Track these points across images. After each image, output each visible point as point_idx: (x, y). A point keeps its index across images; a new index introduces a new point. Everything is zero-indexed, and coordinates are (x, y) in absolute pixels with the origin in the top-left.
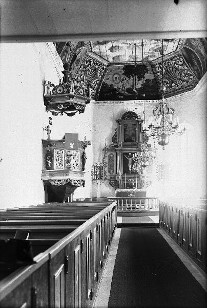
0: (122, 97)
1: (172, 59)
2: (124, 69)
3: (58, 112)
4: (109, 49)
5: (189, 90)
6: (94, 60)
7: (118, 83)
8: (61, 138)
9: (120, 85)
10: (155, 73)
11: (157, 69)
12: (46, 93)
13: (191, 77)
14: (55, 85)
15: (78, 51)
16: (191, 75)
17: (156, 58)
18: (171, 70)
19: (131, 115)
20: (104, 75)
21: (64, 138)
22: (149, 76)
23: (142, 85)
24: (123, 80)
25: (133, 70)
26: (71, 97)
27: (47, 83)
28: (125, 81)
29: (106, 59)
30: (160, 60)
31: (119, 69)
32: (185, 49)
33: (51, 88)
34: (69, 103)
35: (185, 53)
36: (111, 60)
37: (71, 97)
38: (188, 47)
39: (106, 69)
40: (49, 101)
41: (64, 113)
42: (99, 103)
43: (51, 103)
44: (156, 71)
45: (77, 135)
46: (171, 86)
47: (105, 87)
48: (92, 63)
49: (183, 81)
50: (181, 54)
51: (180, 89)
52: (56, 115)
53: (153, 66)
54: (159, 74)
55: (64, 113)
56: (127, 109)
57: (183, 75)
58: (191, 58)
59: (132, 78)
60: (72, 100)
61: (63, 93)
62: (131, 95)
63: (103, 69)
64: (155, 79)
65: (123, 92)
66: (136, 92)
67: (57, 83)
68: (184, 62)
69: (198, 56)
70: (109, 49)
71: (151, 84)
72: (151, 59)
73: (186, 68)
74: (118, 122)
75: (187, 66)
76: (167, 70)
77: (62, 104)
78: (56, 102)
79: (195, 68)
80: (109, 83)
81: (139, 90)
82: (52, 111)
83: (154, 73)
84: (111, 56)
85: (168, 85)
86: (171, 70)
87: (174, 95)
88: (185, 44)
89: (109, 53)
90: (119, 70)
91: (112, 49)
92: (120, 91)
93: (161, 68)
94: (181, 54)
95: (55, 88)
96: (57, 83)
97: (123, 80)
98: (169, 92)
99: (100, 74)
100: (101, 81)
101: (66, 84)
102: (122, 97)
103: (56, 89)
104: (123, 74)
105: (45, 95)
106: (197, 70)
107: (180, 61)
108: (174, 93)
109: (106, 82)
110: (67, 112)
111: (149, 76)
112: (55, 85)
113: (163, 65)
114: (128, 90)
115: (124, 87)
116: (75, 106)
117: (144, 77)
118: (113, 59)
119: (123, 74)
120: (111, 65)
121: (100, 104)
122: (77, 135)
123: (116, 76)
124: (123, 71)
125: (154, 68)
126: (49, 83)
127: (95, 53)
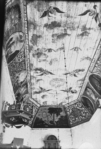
0: (47, 126)
1: (75, 104)
2: (48, 109)
3: (10, 125)
4: (42, 97)
5: (87, 121)
6: (32, 103)
7: (45, 118)
8: (10, 143)
9: (46, 119)
10: (66, 112)
11: (67, 110)
12: (4, 109)
13: (87, 114)
14: (10, 104)
15: (24, 96)
16: (87, 113)
17: (67, 103)
18: (75, 110)
19: (52, 138)
20: (37, 112)
21: (12, 143)
22: (62, 114)
23: (59, 119)
24: (48, 116)
25: (54, 110)
26: (21, 112)
27: (5, 103)
28: (49, 117)
29: (39, 103)
30: (93, 64)
31: (46, 109)
32: (83, 97)
33: (8, 106)
34: (19, 116)
35: (83, 101)
36: (42, 104)
37: (21, 112)
38: (84, 96)
39: (38, 110)
40: (5, 115)
41: (13, 126)
42: (33, 129)
43: (6, 116)
44: (67, 111)
45: (22, 140)
46: (75, 120)
47: (37, 120)
48: (31, 105)
49: (82, 116)
50: (81, 101)
51: (81, 121)
52: (8, 127)
53: (65, 108)
54: (68, 113)
55: (13, 126)
56: (49, 134)
57: (82, 113)
58: (86, 102)
59: (53, 114)
60: (21, 114)
61: (15, 109)
62: (52, 125)
63: (37, 109)
64: (66, 116)
65: (48, 123)
66: (55, 123)
67: (12, 103)
68: (82, 105)
69: (91, 101)
70: (42, 97)
71: (64, 119)
72: (63, 104)
73: (83, 109)
74: (44, 142)
75: (84, 108)
76: (73, 111)
77: (14, 117)
78: (9, 116)
79: (89, 108)
80: (40, 117)
81: (57, 122)
82: (6, 124)
83: (65, 112)
84: (42, 101)
85: (74, 119)
86: (75, 110)
87: (78, 125)
88: (83, 95)
89: (41, 99)
90: (46, 110)
91: (43, 97)
92: (46, 122)
93: (69, 109)
94: (81, 101)
95: (11, 106)
96: (12, 103)
97: (48, 116)
98: (74, 124)
99: (35, 112)
100: (35, 116)
101: (18, 104)
102: (47, 126)
103: (11, 107)
104: (48, 112)
105: (3, 110)
106: (91, 109)
107: (80, 105)
108: (78, 124)
109: (38, 117)
110: (16, 125)
111: (62, 114)
112: (10, 104)
113: (70, 108)
114: (51, 122)
115: (49, 120)
116: (23, 119)
117: (60, 115)
118: (43, 103)
119: (48, 112)
120: (42, 106)
121: (34, 130)
122: (22, 140)
123: (44, 113)
124: (48, 111)
125: (65, 110)
126: (7, 102)
127: (34, 99)
